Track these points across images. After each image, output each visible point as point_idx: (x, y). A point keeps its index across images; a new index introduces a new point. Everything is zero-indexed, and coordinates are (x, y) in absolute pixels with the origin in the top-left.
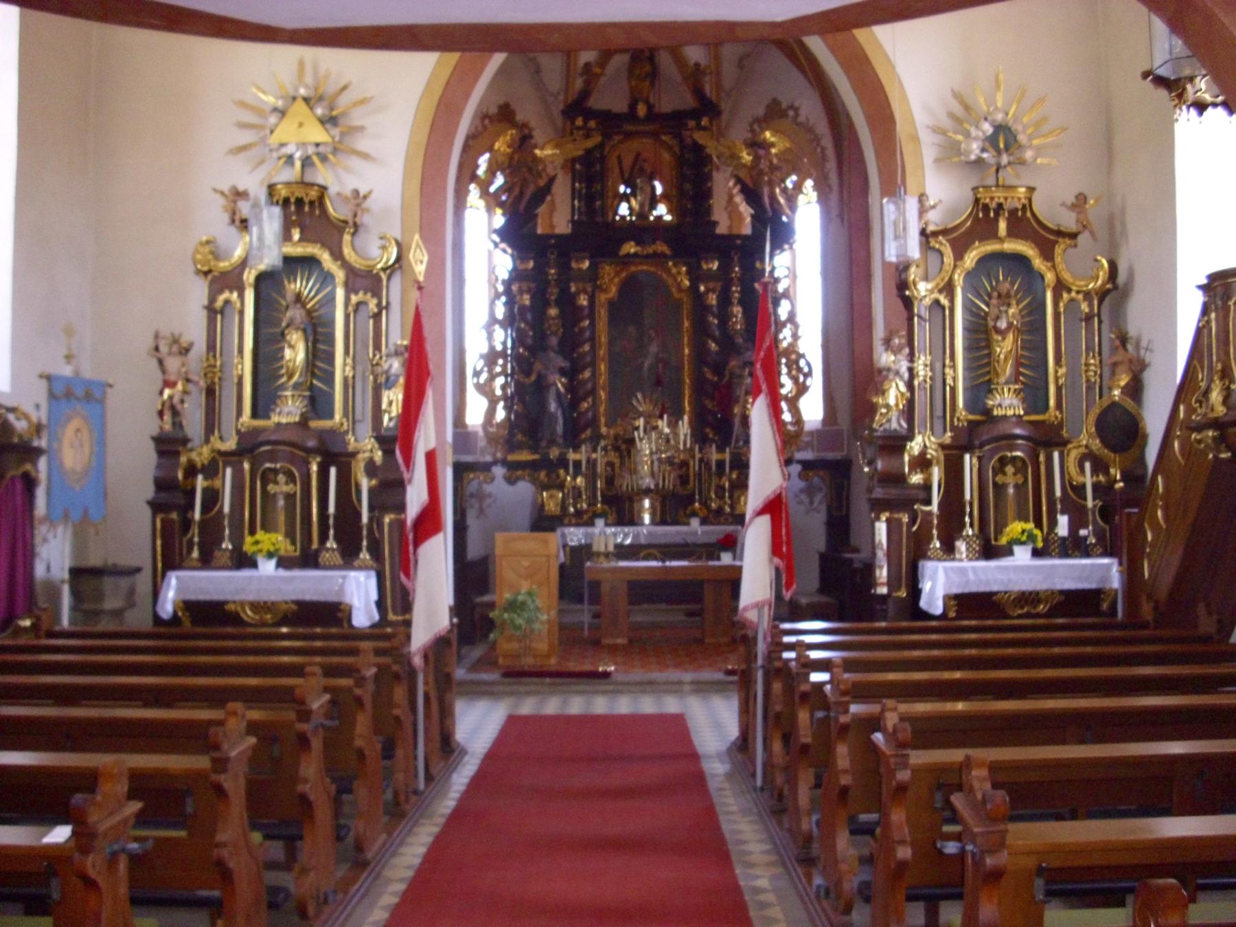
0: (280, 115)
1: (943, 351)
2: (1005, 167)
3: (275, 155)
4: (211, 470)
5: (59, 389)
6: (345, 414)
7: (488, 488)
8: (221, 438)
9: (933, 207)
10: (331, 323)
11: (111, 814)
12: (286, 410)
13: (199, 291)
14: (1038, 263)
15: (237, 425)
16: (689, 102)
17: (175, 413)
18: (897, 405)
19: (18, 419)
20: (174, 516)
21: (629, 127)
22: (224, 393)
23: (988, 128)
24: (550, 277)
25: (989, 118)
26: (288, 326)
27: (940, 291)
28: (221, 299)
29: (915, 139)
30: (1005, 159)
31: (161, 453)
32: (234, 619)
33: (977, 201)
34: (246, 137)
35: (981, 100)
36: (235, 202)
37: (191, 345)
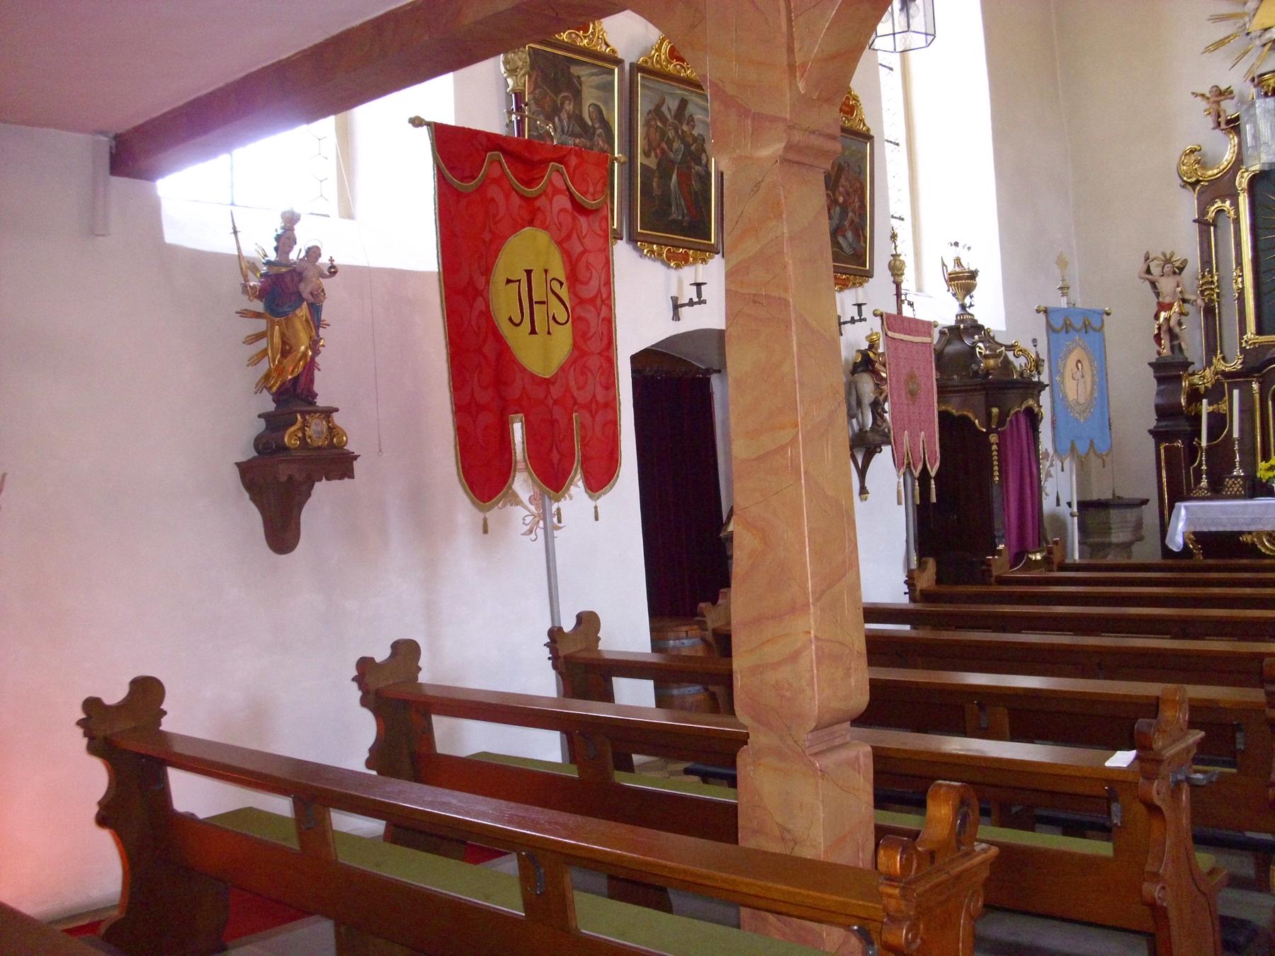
4: (1216, 393)
5: (1058, 322)
8: (1224, 358)
11: (1174, 741)
13: (1188, 204)
15: (1241, 344)
17: (1173, 336)
19: (1017, 357)
20: (1179, 444)
22: (1224, 310)
31: (1160, 380)
32: (1252, 550)
34: (1223, 30)
36: (1218, 103)
37: (1185, 262)
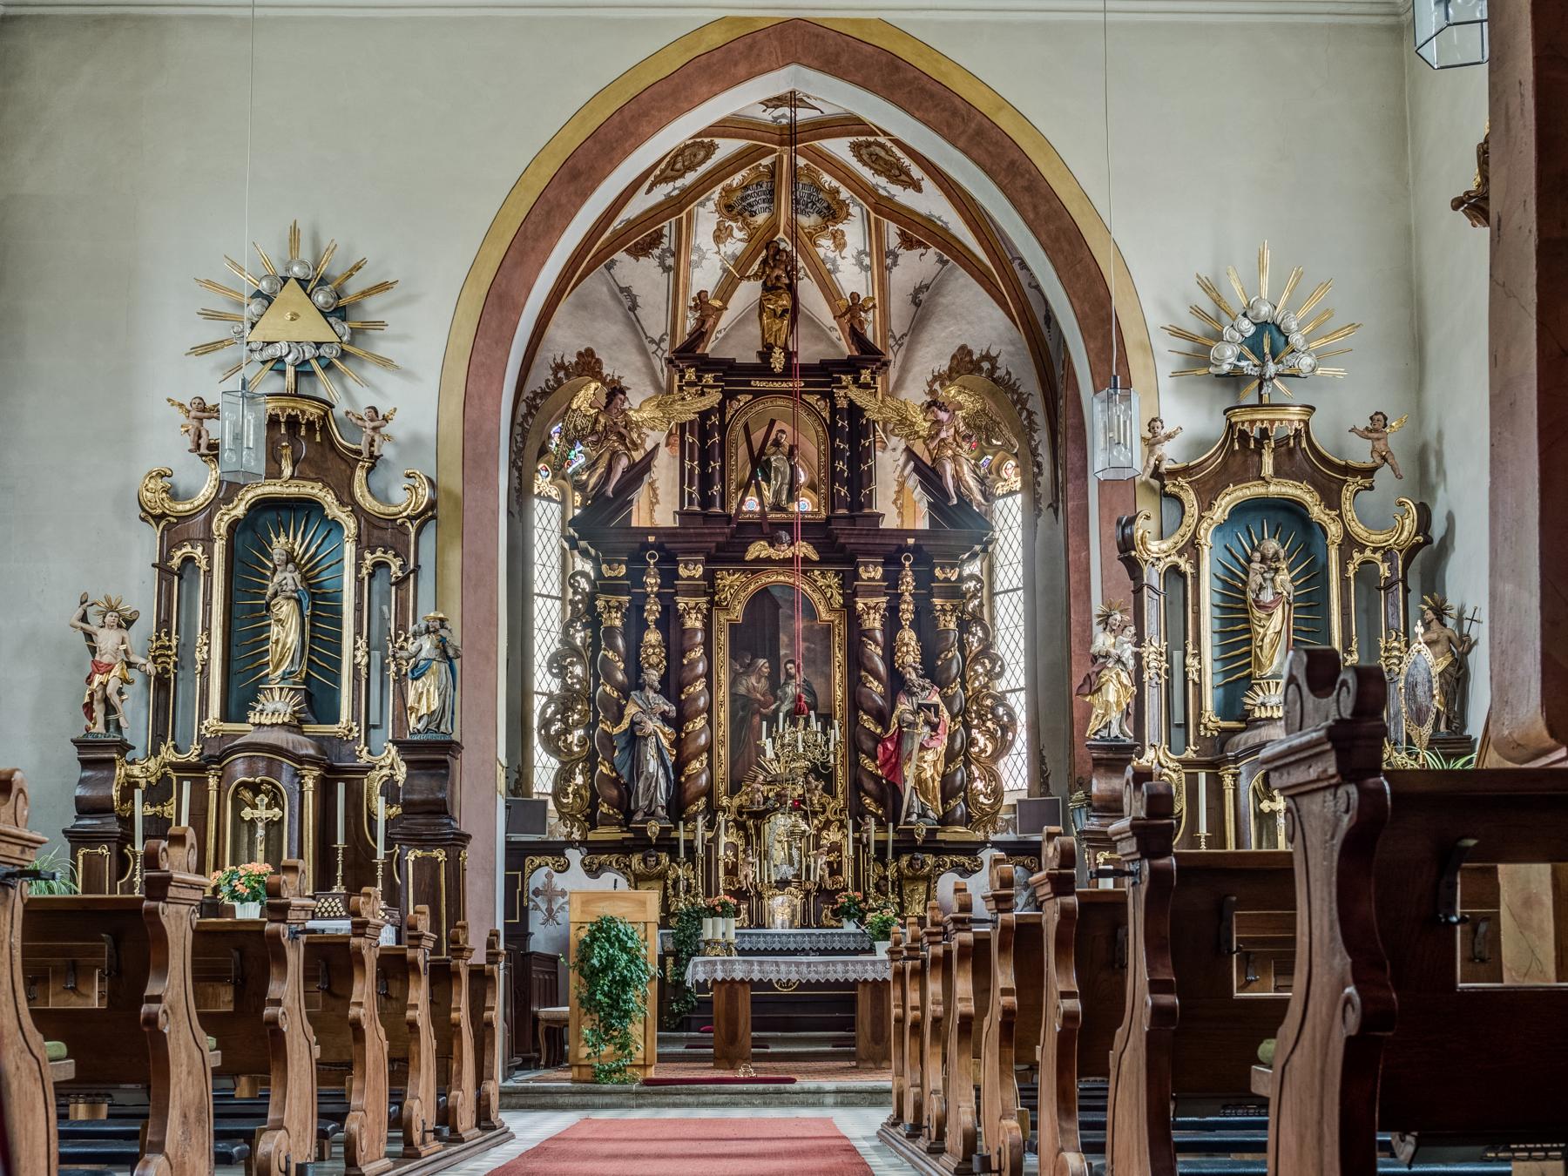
0: (266, 303)
1: (1181, 633)
2: (1271, 379)
3: (257, 356)
6: (355, 717)
7: (560, 881)
8: (176, 748)
9: (1169, 437)
10: (337, 596)
12: (270, 707)
13: (148, 540)
14: (1317, 512)
16: (846, 349)
17: (110, 709)
18: (1118, 704)
21: (758, 384)
23: (1248, 328)
24: (649, 589)
25: (1250, 314)
26: (275, 595)
27: (1180, 553)
28: (178, 555)
29: (1148, 349)
30: (1271, 368)
33: (1231, 426)
35: (1237, 287)
